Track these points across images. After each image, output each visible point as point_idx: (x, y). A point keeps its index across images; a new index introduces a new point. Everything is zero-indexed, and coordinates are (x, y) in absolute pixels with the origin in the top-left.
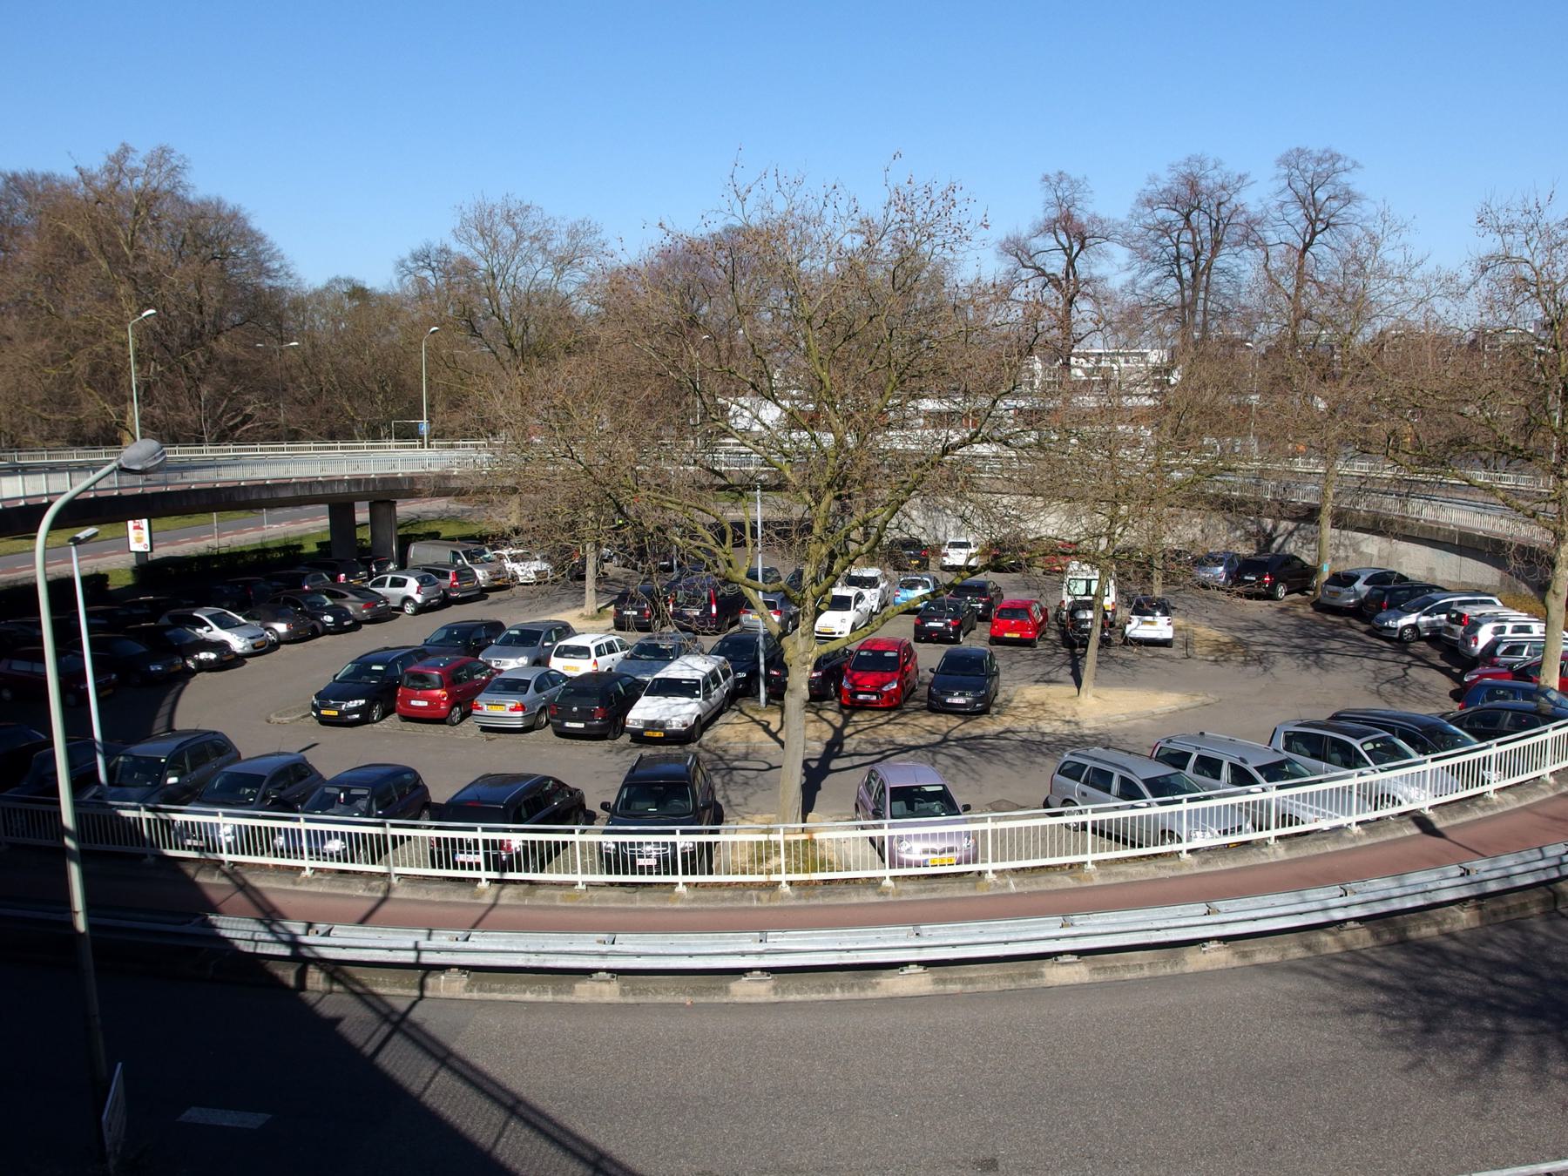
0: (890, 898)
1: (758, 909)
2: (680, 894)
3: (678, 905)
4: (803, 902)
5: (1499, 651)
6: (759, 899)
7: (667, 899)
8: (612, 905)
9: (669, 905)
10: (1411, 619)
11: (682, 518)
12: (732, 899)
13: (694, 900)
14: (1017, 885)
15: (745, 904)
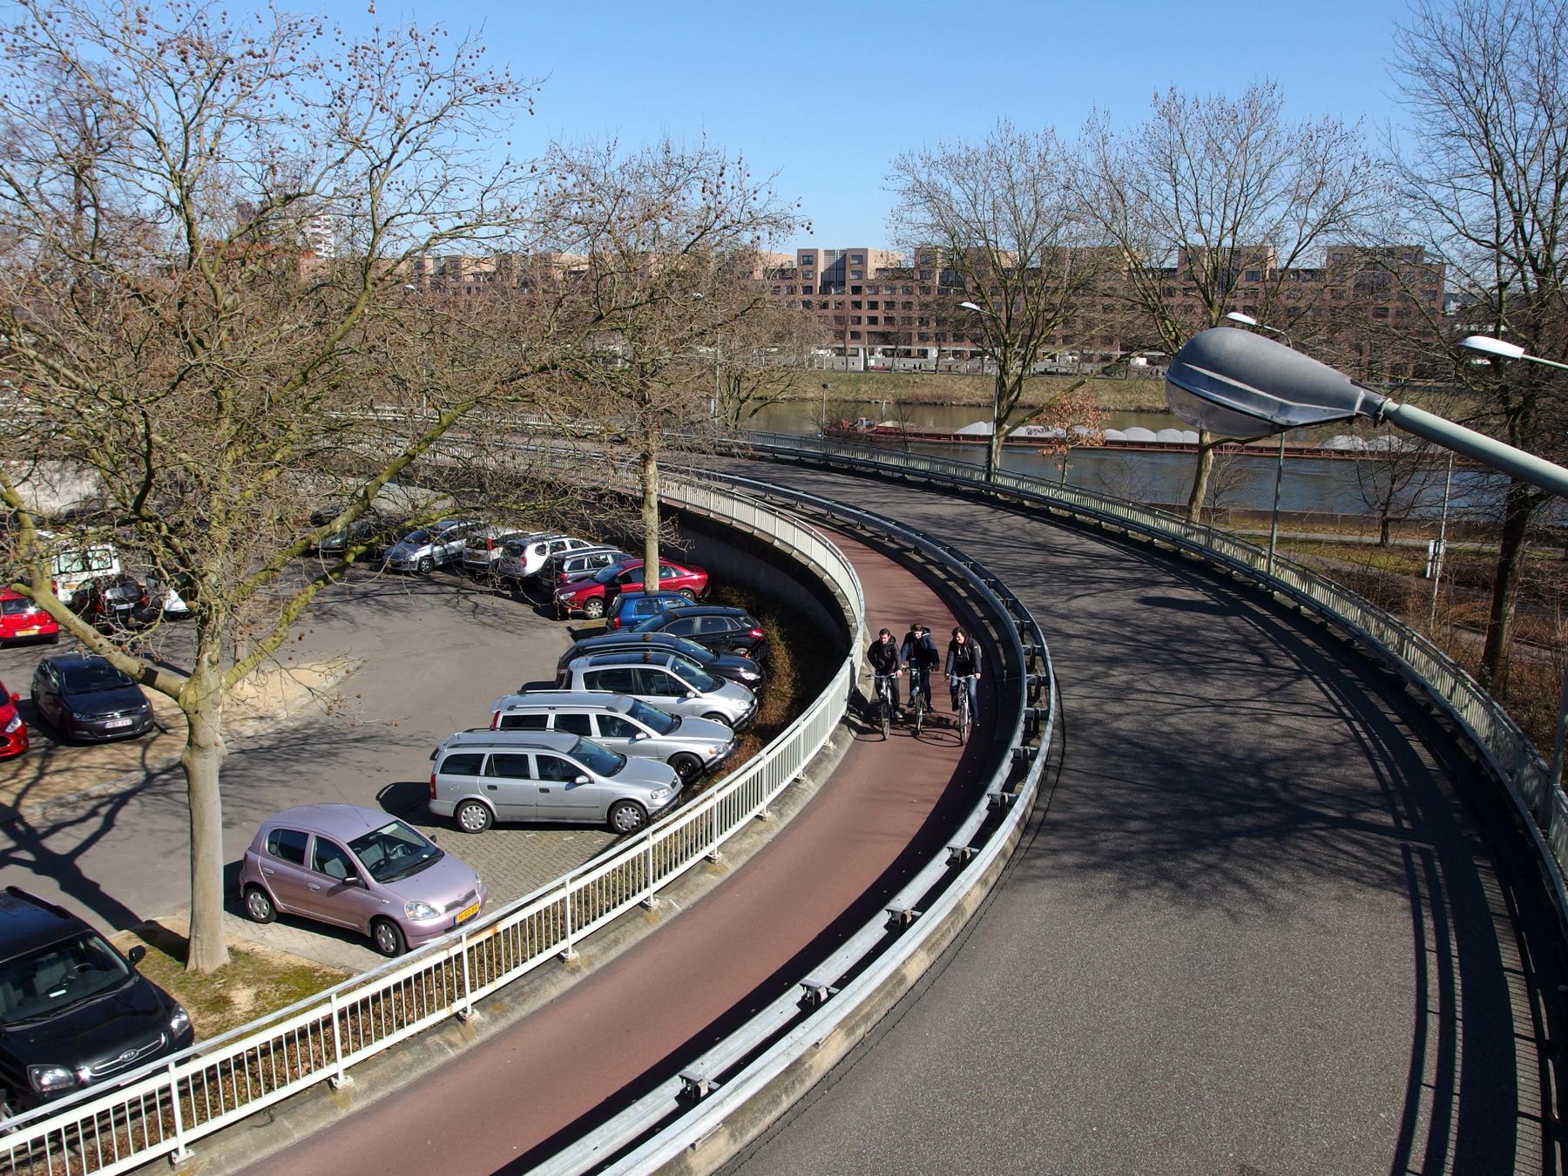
0: (586, 972)
1: (462, 1059)
2: (347, 1090)
3: (356, 1106)
4: (503, 1024)
5: (566, 567)
6: (451, 1045)
7: (333, 1106)
8: (256, 1157)
9: (343, 1113)
10: (425, 551)
11: (548, 312)
12: (420, 1062)
13: (372, 1087)
14: (677, 902)
15: (440, 1060)
